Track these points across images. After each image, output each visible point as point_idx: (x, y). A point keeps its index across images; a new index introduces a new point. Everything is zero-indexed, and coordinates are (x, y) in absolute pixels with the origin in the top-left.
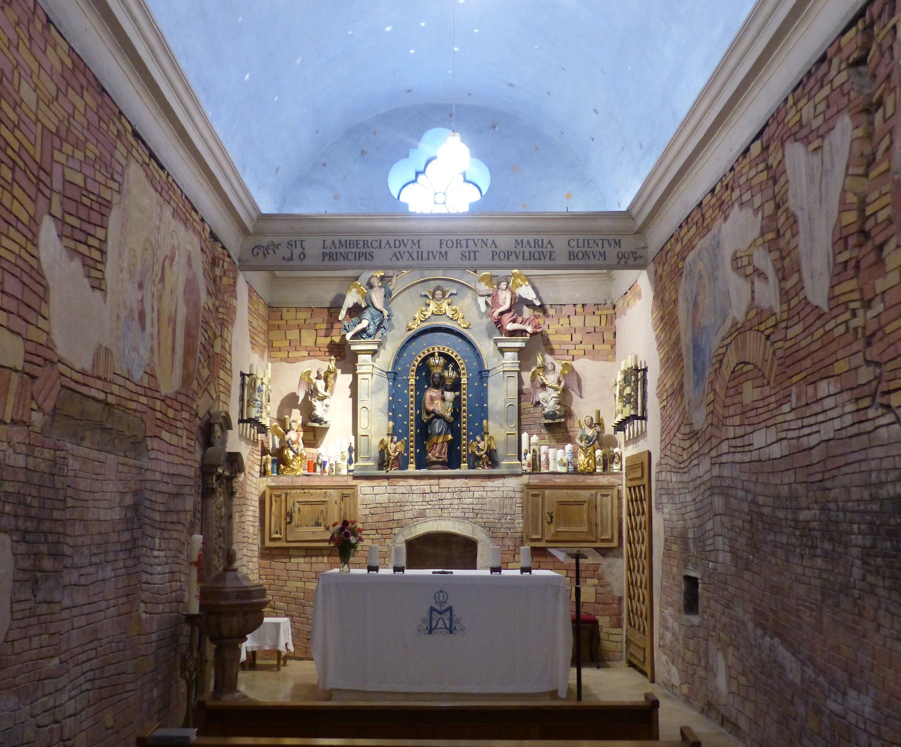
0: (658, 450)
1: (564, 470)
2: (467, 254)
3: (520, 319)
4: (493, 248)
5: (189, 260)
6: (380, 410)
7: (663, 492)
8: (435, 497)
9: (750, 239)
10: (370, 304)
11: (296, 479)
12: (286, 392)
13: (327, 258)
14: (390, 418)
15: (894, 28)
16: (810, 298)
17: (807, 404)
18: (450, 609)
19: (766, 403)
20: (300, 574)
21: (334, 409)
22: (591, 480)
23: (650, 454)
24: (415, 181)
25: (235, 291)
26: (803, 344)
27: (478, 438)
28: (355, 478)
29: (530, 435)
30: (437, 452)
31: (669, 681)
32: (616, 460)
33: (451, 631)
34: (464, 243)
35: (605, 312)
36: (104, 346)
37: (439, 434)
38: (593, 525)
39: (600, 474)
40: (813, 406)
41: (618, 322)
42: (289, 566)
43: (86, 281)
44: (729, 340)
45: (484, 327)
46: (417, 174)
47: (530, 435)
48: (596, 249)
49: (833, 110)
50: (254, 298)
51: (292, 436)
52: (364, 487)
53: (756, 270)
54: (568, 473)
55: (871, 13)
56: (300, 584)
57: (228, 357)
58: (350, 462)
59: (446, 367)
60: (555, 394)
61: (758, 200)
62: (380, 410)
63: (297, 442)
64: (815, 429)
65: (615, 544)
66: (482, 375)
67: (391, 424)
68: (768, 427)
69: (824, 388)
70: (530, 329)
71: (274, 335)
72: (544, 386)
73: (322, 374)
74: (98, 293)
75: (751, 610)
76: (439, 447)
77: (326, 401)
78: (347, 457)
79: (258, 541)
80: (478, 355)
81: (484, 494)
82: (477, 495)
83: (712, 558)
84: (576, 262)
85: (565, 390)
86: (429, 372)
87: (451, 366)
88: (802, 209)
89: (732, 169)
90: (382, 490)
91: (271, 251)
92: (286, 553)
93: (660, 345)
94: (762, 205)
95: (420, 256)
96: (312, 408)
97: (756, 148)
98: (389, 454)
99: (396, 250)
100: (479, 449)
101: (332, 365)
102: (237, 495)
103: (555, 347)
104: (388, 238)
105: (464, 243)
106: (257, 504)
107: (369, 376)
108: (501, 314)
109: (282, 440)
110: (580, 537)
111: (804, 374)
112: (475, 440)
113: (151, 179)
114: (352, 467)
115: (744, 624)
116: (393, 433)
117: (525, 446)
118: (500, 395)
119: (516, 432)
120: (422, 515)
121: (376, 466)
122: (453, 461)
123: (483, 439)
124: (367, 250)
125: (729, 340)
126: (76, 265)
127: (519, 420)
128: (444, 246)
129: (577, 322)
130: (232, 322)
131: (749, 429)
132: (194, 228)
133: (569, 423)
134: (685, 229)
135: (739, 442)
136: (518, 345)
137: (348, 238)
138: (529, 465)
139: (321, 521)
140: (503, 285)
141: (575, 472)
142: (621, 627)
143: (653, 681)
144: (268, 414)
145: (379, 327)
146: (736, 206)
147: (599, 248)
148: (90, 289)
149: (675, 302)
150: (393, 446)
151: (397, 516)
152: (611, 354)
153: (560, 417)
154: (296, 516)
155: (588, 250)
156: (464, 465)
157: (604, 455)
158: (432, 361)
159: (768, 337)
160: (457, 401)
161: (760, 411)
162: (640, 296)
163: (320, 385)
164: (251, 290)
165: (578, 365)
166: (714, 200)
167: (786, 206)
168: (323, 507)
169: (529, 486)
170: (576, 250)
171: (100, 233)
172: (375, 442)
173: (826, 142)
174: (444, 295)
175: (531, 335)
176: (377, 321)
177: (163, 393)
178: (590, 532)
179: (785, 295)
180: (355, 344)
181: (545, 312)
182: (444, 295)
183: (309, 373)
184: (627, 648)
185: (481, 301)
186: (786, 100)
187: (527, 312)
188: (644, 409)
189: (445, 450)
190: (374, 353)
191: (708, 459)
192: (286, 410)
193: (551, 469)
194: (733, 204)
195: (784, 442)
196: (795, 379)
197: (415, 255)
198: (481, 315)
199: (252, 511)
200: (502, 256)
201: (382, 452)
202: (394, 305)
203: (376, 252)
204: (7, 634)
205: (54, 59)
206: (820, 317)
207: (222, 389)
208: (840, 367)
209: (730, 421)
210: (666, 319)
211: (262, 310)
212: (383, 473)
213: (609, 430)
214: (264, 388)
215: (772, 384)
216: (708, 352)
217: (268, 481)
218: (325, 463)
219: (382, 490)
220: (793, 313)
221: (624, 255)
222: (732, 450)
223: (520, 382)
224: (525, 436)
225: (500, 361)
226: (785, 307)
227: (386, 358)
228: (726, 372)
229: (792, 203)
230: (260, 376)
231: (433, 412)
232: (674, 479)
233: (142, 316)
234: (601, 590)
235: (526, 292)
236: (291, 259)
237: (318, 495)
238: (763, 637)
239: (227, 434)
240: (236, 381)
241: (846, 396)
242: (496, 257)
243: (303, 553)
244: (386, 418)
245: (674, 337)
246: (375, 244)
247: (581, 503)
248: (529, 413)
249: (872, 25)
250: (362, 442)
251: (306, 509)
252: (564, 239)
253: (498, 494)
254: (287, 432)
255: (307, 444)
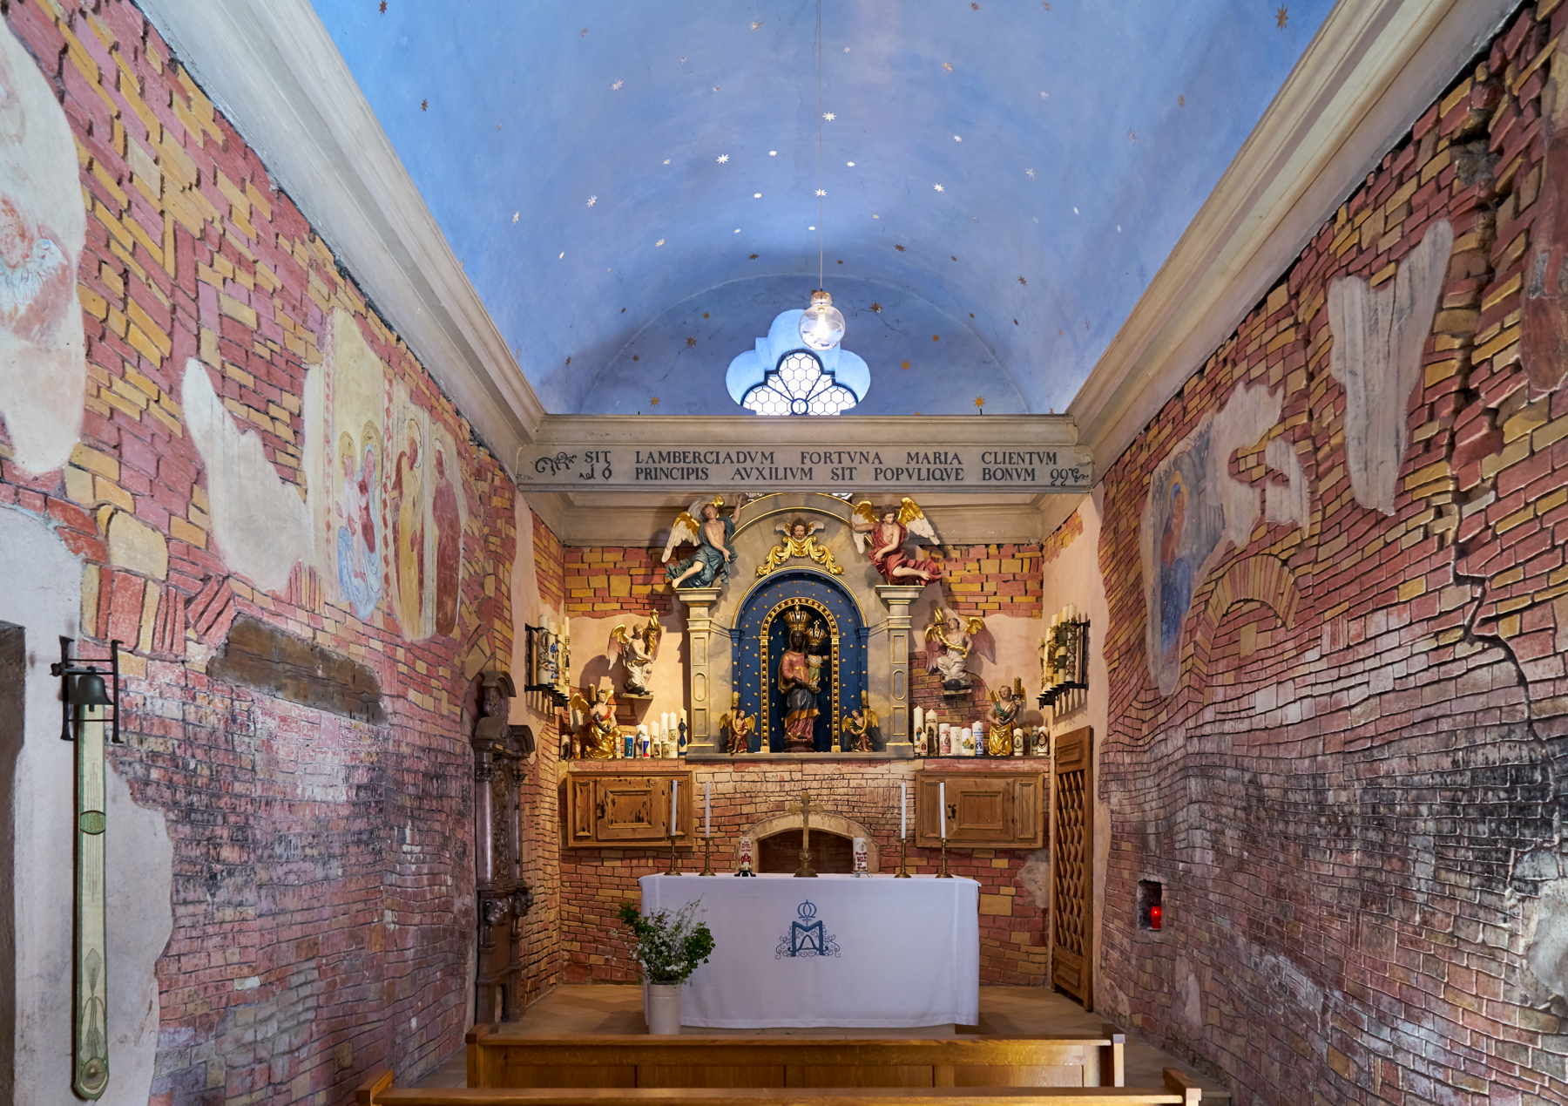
0: (1105, 726)
1: (971, 753)
2: (840, 472)
3: (912, 562)
4: (877, 465)
5: (440, 463)
6: (722, 677)
7: (1110, 777)
8: (798, 786)
9: (1262, 429)
10: (705, 542)
11: (607, 764)
12: (592, 656)
13: (642, 476)
14: (734, 688)
15: (1547, 65)
16: (1360, 499)
17: (1349, 647)
18: (820, 924)
19: (1279, 651)
20: (617, 881)
21: (659, 676)
22: (1006, 766)
23: (1091, 730)
24: (765, 383)
25: (513, 517)
26: (1345, 564)
27: (855, 713)
28: (689, 762)
29: (925, 711)
30: (801, 725)
31: (1114, 1010)
32: (1042, 741)
33: (821, 951)
34: (835, 457)
35: (1028, 554)
36: (306, 565)
37: (802, 708)
38: (1009, 821)
39: (1019, 758)
40: (1360, 648)
41: (1046, 567)
42: (600, 870)
43: (270, 466)
44: (1221, 572)
45: (862, 572)
46: (767, 374)
47: (925, 711)
48: (1021, 466)
49: (1420, 216)
50: (542, 531)
51: (601, 709)
52: (701, 774)
53: (1269, 471)
54: (976, 757)
55: (1501, 50)
56: (618, 893)
57: (506, 602)
58: (681, 742)
59: (810, 625)
60: (959, 659)
61: (1276, 373)
62: (722, 677)
63: (607, 717)
64: (1359, 679)
65: (1040, 844)
66: (860, 634)
67: (736, 695)
68: (1279, 683)
69: (1379, 622)
70: (925, 575)
71: (572, 582)
72: (944, 649)
73: (641, 631)
74: (290, 487)
75: (1244, 922)
76: (801, 725)
77: (648, 667)
78: (677, 737)
79: (558, 840)
80: (854, 609)
81: (863, 782)
82: (853, 783)
83: (1184, 858)
84: (993, 482)
85: (972, 653)
86: (787, 630)
87: (817, 623)
88: (1353, 373)
89: (1235, 334)
90: (726, 777)
91: (562, 466)
92: (597, 854)
93: (1110, 591)
94: (1285, 377)
95: (774, 474)
96: (629, 675)
97: (1280, 297)
98: (734, 733)
99: (740, 466)
100: (856, 727)
101: (654, 620)
102: (526, 781)
103: (960, 599)
104: (727, 449)
105: (835, 457)
106: (556, 794)
107: (706, 635)
108: (887, 555)
109: (586, 715)
110: (992, 835)
111: (1346, 605)
112: (851, 716)
113: (372, 340)
114: (684, 749)
115: (1232, 939)
116: (739, 706)
117: (918, 723)
118: (885, 661)
119: (905, 705)
120: (780, 808)
121: (717, 748)
122: (821, 741)
123: (861, 715)
124: (700, 466)
125: (1221, 572)
126: (252, 440)
127: (911, 691)
128: (807, 460)
129: (990, 567)
130: (512, 558)
131: (1248, 688)
132: (445, 423)
133: (979, 695)
134: (1154, 431)
135: (1230, 707)
136: (909, 595)
137: (672, 449)
138: (923, 747)
139: (643, 815)
140: (889, 517)
141: (986, 754)
142: (1045, 944)
143: (1090, 1010)
144: (567, 682)
145: (717, 573)
146: (1240, 386)
147: (1027, 465)
148: (279, 482)
149: (1136, 530)
150: (740, 723)
151: (746, 809)
152: (1036, 607)
153: (966, 688)
154: (609, 809)
155: (1009, 467)
156: (836, 748)
157: (1025, 736)
158: (791, 616)
159: (1285, 562)
160: (826, 668)
161: (1268, 663)
162: (1080, 529)
163: (639, 645)
164: (538, 521)
165: (989, 621)
166: (1204, 383)
167: (1325, 374)
168: (645, 799)
169: (922, 772)
170: (993, 467)
171: (289, 401)
172: (715, 718)
173: (1404, 267)
174: (807, 530)
175: (927, 582)
176: (715, 564)
177: (408, 640)
178: (1005, 830)
179: (1317, 501)
180: (685, 593)
181: (946, 555)
182: (807, 530)
183: (623, 630)
184: (1054, 970)
185: (859, 539)
186: (1335, 218)
187: (921, 554)
188: (1084, 674)
189: (810, 728)
190: (712, 605)
191: (1182, 732)
192: (592, 678)
193: (954, 752)
194: (1234, 385)
195: (1305, 701)
196: (1328, 615)
197: (766, 473)
198: (858, 557)
199: (548, 803)
200: (889, 474)
201: (724, 730)
202: (738, 544)
203: (712, 468)
204: (168, 946)
205: (194, 119)
206: (1378, 523)
207: (498, 643)
208: (1405, 593)
209: (1220, 680)
210: (1120, 553)
211: (554, 548)
212: (727, 756)
213: (1032, 703)
214: (560, 647)
215: (1291, 625)
216: (1185, 592)
217: (566, 768)
218: (646, 743)
219: (726, 777)
220: (1327, 524)
221: (1060, 474)
222: (1219, 717)
223: (912, 643)
224: (918, 711)
225: (887, 617)
226: (1318, 516)
227: (729, 611)
228: (1213, 615)
229: (1335, 369)
230: (553, 631)
231: (793, 680)
232: (1127, 760)
233: (368, 529)
234: (1019, 901)
235: (920, 527)
236: (592, 476)
237: (638, 783)
238: (1261, 955)
239: (508, 703)
240: (519, 638)
241: (1418, 630)
242: (881, 476)
243: (621, 854)
244: (728, 688)
245: (1132, 578)
246: (710, 458)
247: (995, 794)
248: (923, 682)
249: (1499, 74)
250: (698, 719)
251: (622, 800)
252: (977, 452)
253: (883, 783)
254: (592, 704)
255: (621, 721)
